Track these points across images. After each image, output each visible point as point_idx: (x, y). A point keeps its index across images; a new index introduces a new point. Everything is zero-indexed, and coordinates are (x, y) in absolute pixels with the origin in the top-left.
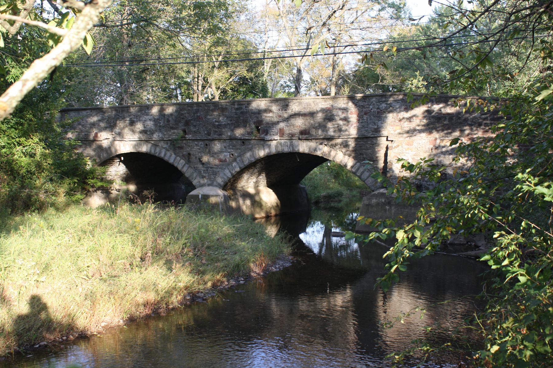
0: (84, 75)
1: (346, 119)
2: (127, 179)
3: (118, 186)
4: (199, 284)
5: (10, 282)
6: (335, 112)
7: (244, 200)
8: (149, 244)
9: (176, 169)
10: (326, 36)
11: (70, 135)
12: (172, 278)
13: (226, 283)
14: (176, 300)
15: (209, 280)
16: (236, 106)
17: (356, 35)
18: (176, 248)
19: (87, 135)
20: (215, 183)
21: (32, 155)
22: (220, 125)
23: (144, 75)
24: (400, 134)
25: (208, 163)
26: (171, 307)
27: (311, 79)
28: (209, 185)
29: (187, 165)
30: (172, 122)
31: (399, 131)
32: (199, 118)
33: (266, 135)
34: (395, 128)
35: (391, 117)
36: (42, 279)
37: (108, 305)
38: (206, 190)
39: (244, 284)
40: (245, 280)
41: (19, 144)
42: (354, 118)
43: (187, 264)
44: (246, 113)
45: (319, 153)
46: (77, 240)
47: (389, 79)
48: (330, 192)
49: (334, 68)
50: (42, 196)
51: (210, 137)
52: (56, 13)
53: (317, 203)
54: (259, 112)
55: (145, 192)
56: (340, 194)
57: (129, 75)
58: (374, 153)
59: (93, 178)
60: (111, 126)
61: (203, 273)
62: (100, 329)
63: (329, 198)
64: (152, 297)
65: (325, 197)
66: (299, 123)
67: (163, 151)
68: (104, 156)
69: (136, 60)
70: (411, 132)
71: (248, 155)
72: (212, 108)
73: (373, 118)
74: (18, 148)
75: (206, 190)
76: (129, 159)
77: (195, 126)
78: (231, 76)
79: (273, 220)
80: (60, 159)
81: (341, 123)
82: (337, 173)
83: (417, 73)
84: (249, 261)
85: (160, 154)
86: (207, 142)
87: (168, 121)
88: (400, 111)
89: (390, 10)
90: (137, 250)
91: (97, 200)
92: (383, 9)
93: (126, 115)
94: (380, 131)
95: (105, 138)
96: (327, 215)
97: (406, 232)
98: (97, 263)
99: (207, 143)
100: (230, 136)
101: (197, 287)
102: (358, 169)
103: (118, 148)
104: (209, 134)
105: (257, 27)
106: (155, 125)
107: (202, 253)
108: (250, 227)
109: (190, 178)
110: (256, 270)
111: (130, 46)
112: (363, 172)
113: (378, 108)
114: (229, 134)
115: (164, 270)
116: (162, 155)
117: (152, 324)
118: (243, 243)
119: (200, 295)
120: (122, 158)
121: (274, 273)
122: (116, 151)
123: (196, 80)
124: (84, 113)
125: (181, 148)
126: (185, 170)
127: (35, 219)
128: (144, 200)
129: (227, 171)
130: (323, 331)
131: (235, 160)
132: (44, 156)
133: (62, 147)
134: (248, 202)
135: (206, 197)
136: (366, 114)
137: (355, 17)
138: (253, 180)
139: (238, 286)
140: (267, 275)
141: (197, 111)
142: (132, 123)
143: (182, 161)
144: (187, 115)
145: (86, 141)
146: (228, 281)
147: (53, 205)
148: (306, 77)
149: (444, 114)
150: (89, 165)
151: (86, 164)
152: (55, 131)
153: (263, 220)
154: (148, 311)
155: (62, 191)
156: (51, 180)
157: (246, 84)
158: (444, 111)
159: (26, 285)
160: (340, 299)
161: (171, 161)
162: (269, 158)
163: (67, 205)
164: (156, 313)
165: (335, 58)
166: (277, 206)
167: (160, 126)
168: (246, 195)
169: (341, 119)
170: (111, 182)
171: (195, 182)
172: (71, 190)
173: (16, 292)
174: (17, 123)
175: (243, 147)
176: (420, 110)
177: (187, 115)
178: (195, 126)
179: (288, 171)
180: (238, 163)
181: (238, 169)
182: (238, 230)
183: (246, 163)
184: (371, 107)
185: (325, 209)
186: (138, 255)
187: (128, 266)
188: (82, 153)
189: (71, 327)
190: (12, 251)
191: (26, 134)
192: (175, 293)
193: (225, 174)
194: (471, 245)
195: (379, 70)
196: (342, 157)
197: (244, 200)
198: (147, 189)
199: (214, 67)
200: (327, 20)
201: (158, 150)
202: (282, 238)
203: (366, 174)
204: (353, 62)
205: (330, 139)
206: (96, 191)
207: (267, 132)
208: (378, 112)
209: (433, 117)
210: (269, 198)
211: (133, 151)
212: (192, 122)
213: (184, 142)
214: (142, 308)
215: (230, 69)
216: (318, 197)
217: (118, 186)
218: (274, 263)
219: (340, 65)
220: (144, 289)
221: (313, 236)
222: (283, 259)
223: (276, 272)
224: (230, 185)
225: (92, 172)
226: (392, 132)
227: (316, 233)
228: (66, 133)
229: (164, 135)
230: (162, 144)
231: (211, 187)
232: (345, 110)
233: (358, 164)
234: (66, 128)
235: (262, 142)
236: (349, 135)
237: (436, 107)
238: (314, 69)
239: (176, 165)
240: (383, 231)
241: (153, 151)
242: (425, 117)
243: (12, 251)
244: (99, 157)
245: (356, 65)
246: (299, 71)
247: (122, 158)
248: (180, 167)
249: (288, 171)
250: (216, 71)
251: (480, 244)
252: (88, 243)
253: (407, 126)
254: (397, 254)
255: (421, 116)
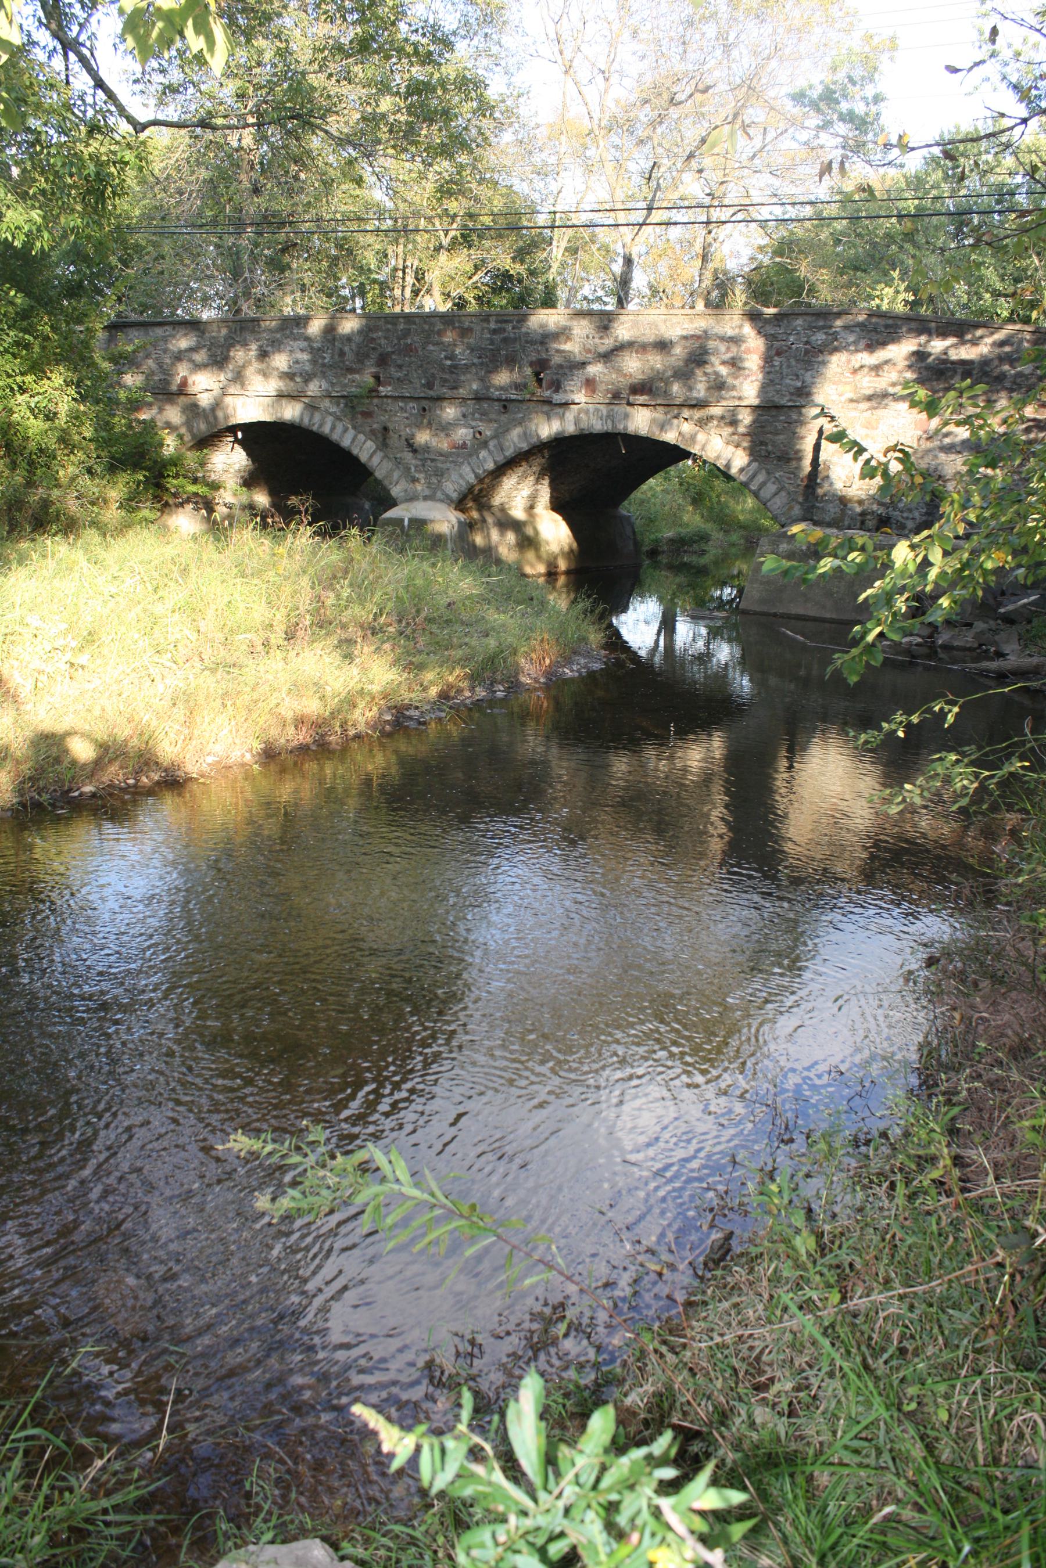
0: (155, 254)
1: (735, 363)
2: (249, 482)
3: (230, 494)
4: (410, 690)
5: (16, 663)
6: (711, 344)
7: (502, 534)
8: (305, 601)
9: (356, 460)
10: (693, 187)
11: (128, 379)
12: (355, 671)
13: (468, 694)
14: (363, 717)
15: (434, 681)
16: (493, 326)
17: (759, 186)
18: (362, 613)
19: (167, 382)
20: (439, 494)
21: (50, 417)
22: (455, 367)
23: (287, 258)
24: (852, 401)
25: (427, 448)
26: (352, 732)
27: (651, 287)
28: (426, 498)
29: (379, 455)
30: (350, 356)
31: (851, 395)
32: (409, 350)
33: (557, 391)
34: (841, 388)
35: (838, 363)
36: (82, 659)
37: (222, 719)
38: (420, 509)
39: (504, 699)
40: (507, 690)
41: (23, 390)
42: (753, 362)
43: (387, 646)
44: (515, 340)
45: (670, 437)
46: (150, 589)
47: (826, 292)
48: (683, 531)
49: (705, 258)
50: (73, 506)
51: (431, 393)
52: (100, 92)
53: (653, 553)
54: (547, 337)
55: (293, 501)
56: (703, 537)
57: (254, 259)
58: (794, 437)
59: (176, 476)
60: (218, 361)
61: (421, 667)
62: (205, 768)
63: (680, 544)
64: (312, 707)
65: (671, 541)
66: (633, 365)
67: (329, 420)
68: (202, 427)
69: (270, 221)
70: (878, 398)
71: (515, 433)
72: (439, 326)
73: (793, 362)
74: (20, 398)
75: (420, 509)
76: (256, 437)
77: (400, 367)
78: (477, 268)
79: (562, 580)
80: (107, 426)
81: (723, 370)
82: (700, 494)
83: (895, 274)
84: (515, 652)
85: (321, 425)
86: (425, 404)
87: (342, 354)
88: (857, 351)
89: (842, 128)
90: (278, 616)
91: (185, 522)
92: (826, 125)
93: (249, 337)
94: (809, 394)
95: (204, 385)
96: (672, 581)
97: (913, 547)
98: (194, 636)
99: (426, 406)
100: (476, 392)
101: (407, 696)
102: (753, 476)
103: (230, 411)
104: (430, 386)
105: (537, 158)
106: (313, 362)
107: (417, 629)
108: (514, 590)
109: (386, 483)
110: (531, 670)
111: (256, 191)
112: (763, 485)
113: (807, 343)
114: (475, 387)
115: (336, 658)
116: (326, 430)
117: (311, 767)
118: (502, 616)
119: (412, 713)
120: (240, 435)
121: (567, 681)
122: (227, 417)
123: (400, 274)
124: (159, 331)
125: (367, 414)
126: (376, 461)
127: (57, 548)
128: (288, 514)
129: (466, 469)
130: (657, 817)
131: (485, 444)
132: (75, 417)
133: (112, 402)
134: (511, 537)
135: (419, 524)
136: (779, 353)
137: (759, 146)
138: (525, 490)
139: (492, 702)
140: (554, 683)
141: (407, 333)
142: (263, 355)
143: (369, 443)
144: (383, 342)
145: (166, 391)
146: (472, 689)
147: (94, 524)
148: (639, 280)
149: (953, 363)
150: (170, 445)
151: (161, 445)
152: (94, 365)
153: (541, 580)
154: (304, 736)
155: (115, 493)
156: (90, 471)
157: (508, 290)
158: (954, 355)
159: (49, 669)
160: (700, 755)
161: (346, 443)
162: (559, 445)
163: (123, 528)
164: (318, 746)
165: (710, 238)
166: (571, 551)
167: (324, 365)
168: (507, 523)
169: (723, 363)
170: (215, 486)
171: (396, 491)
172: (130, 500)
173: (29, 685)
174: (17, 344)
175: (504, 418)
176: (901, 351)
177: (383, 342)
178: (400, 367)
179: (598, 474)
180: (490, 453)
181: (490, 466)
182: (490, 588)
183: (509, 453)
184: (792, 339)
185: (670, 567)
186: (280, 629)
187: (260, 648)
188: (153, 420)
189: (146, 760)
190: (18, 601)
191: (38, 368)
192: (362, 704)
193: (461, 476)
194: (987, 651)
195: (803, 270)
196: (720, 447)
197: (502, 534)
198: (296, 494)
199: (438, 249)
200: (698, 148)
201: (317, 417)
202: (585, 612)
203: (771, 488)
204: (746, 253)
205: (700, 405)
206: (182, 505)
207: (557, 386)
208: (807, 352)
209: (928, 368)
210: (555, 532)
211: (267, 418)
212: (394, 356)
213: (376, 401)
214: (291, 730)
215: (475, 254)
216: (656, 541)
217: (230, 494)
218: (568, 661)
219: (718, 256)
220: (296, 689)
221: (639, 625)
222: (588, 655)
223: (572, 679)
224: (476, 498)
225: (175, 461)
226: (835, 397)
227: (642, 625)
228: (120, 373)
229: (333, 384)
230: (326, 403)
231: (429, 503)
232: (735, 340)
233: (755, 465)
234: (123, 362)
235: (546, 408)
236: (740, 398)
237: (938, 346)
238: (663, 258)
239: (355, 451)
240: (850, 558)
241: (306, 421)
242: (909, 367)
243: (18, 601)
244: (190, 429)
245: (752, 259)
246: (628, 261)
247: (240, 435)
248: (363, 458)
249: (598, 474)
250: (443, 256)
251: (1006, 649)
252: (175, 595)
253: (869, 384)
254: (888, 598)
255: (902, 363)
